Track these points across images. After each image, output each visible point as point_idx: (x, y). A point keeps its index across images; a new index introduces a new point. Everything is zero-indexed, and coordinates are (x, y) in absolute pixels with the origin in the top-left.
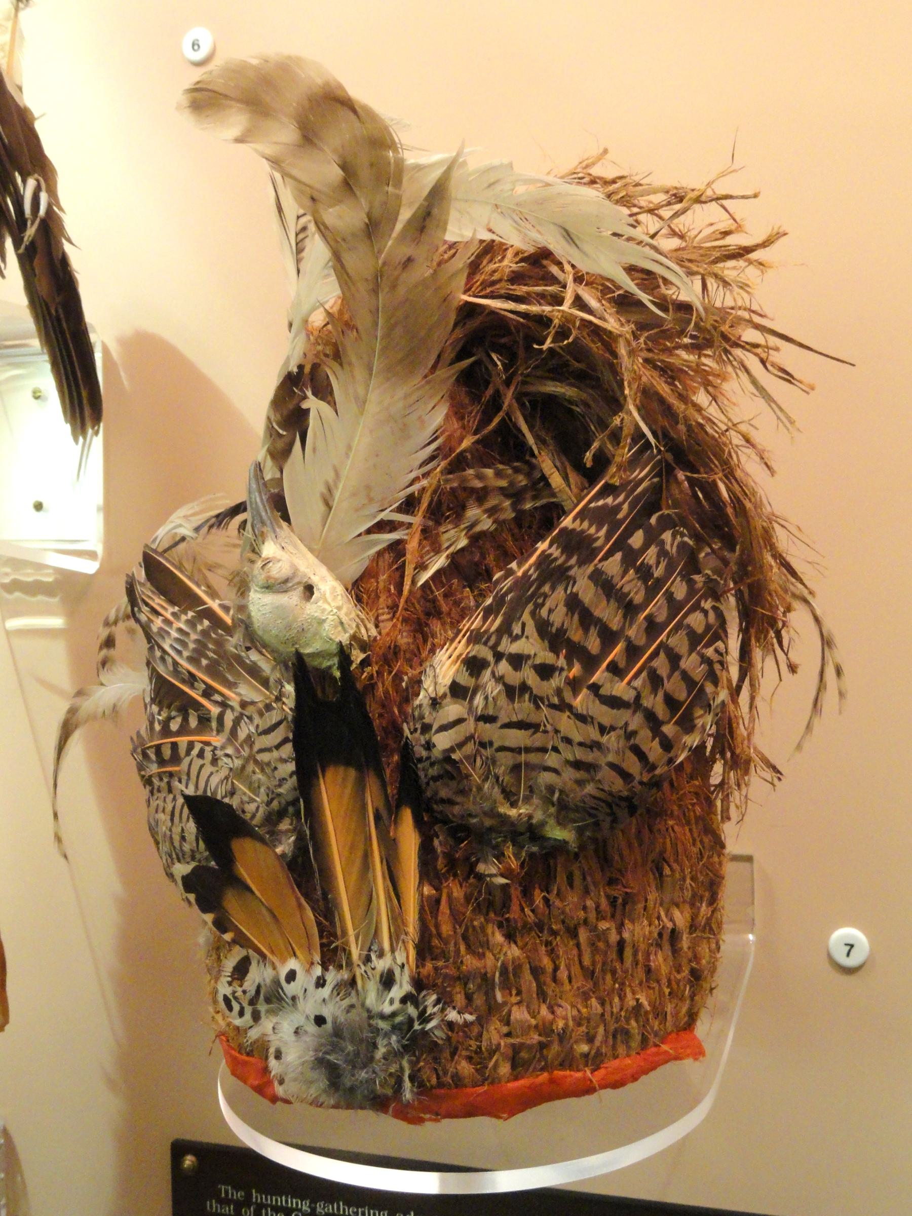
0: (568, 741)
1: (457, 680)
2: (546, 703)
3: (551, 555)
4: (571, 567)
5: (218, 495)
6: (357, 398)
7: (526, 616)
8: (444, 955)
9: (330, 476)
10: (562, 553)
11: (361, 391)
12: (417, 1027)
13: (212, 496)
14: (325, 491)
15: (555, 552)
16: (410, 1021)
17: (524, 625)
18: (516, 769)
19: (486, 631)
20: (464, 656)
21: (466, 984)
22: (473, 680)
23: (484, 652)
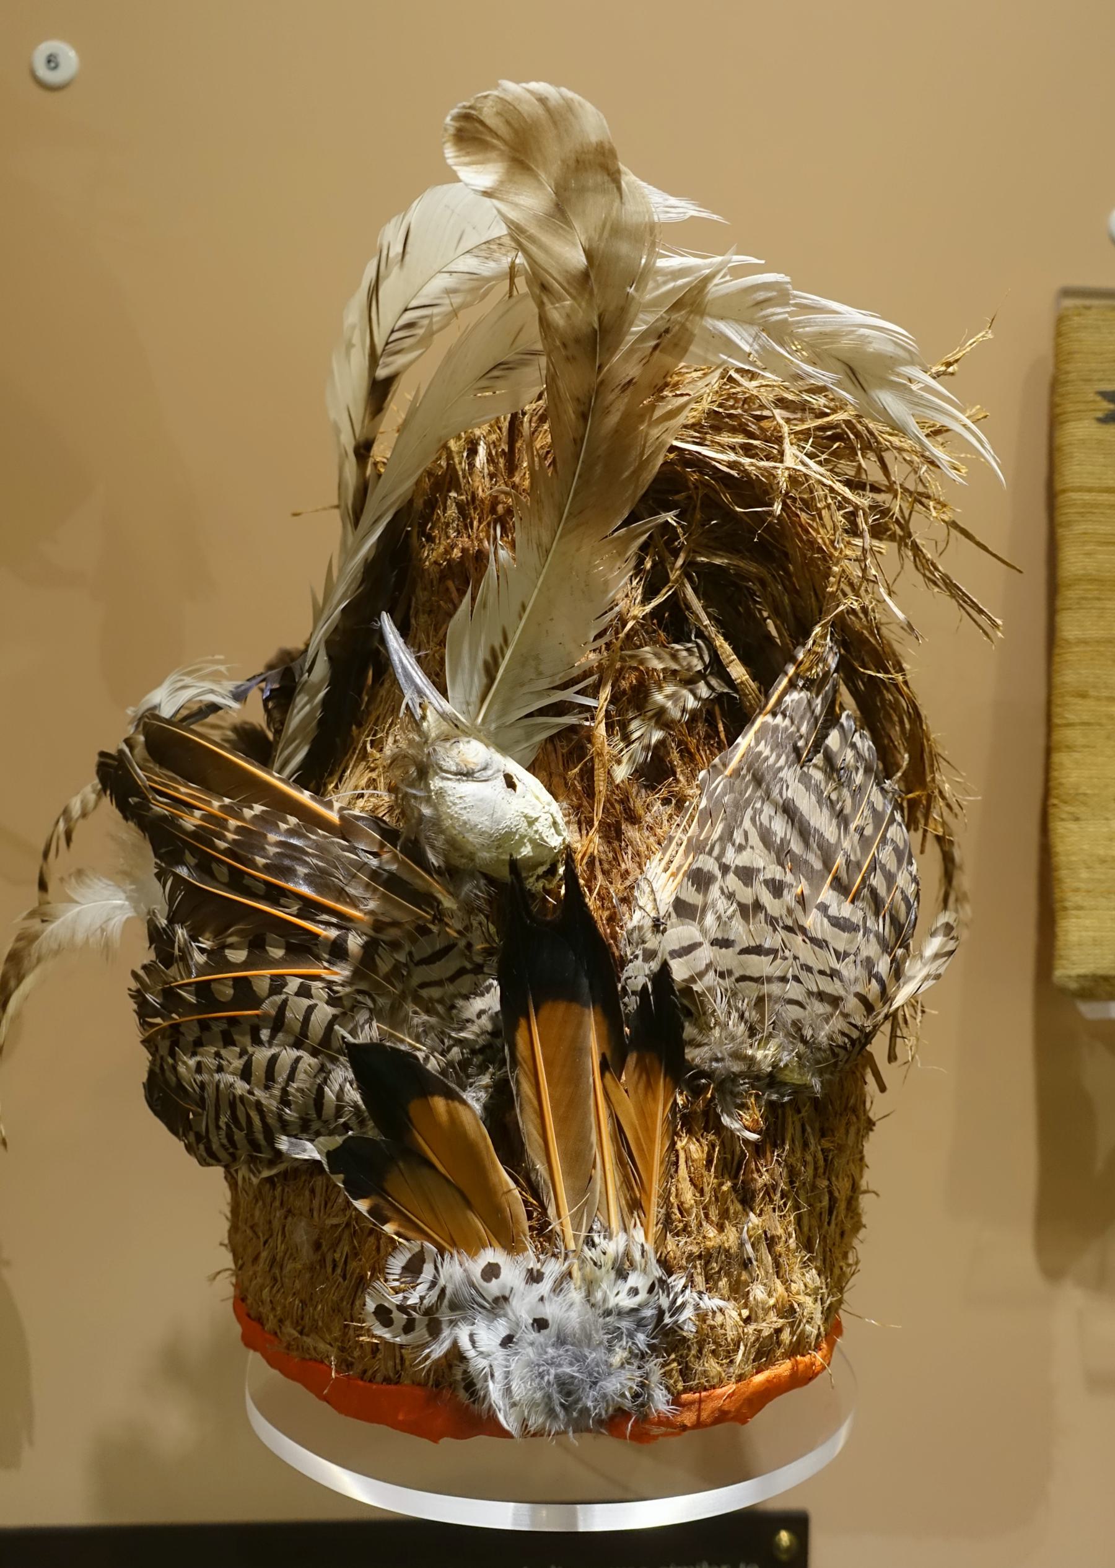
0: (809, 969)
1: (683, 897)
2: (781, 924)
3: (760, 753)
4: (781, 769)
5: (217, 657)
6: (539, 545)
7: (747, 824)
8: (686, 1230)
9: (498, 642)
10: (772, 751)
11: (545, 539)
12: (667, 1320)
13: (210, 658)
14: (489, 659)
15: (764, 749)
16: (661, 1313)
17: (746, 834)
18: (760, 1001)
19: (707, 838)
20: (685, 868)
21: (707, 1263)
22: (701, 897)
23: (708, 864)
